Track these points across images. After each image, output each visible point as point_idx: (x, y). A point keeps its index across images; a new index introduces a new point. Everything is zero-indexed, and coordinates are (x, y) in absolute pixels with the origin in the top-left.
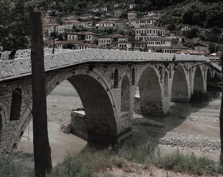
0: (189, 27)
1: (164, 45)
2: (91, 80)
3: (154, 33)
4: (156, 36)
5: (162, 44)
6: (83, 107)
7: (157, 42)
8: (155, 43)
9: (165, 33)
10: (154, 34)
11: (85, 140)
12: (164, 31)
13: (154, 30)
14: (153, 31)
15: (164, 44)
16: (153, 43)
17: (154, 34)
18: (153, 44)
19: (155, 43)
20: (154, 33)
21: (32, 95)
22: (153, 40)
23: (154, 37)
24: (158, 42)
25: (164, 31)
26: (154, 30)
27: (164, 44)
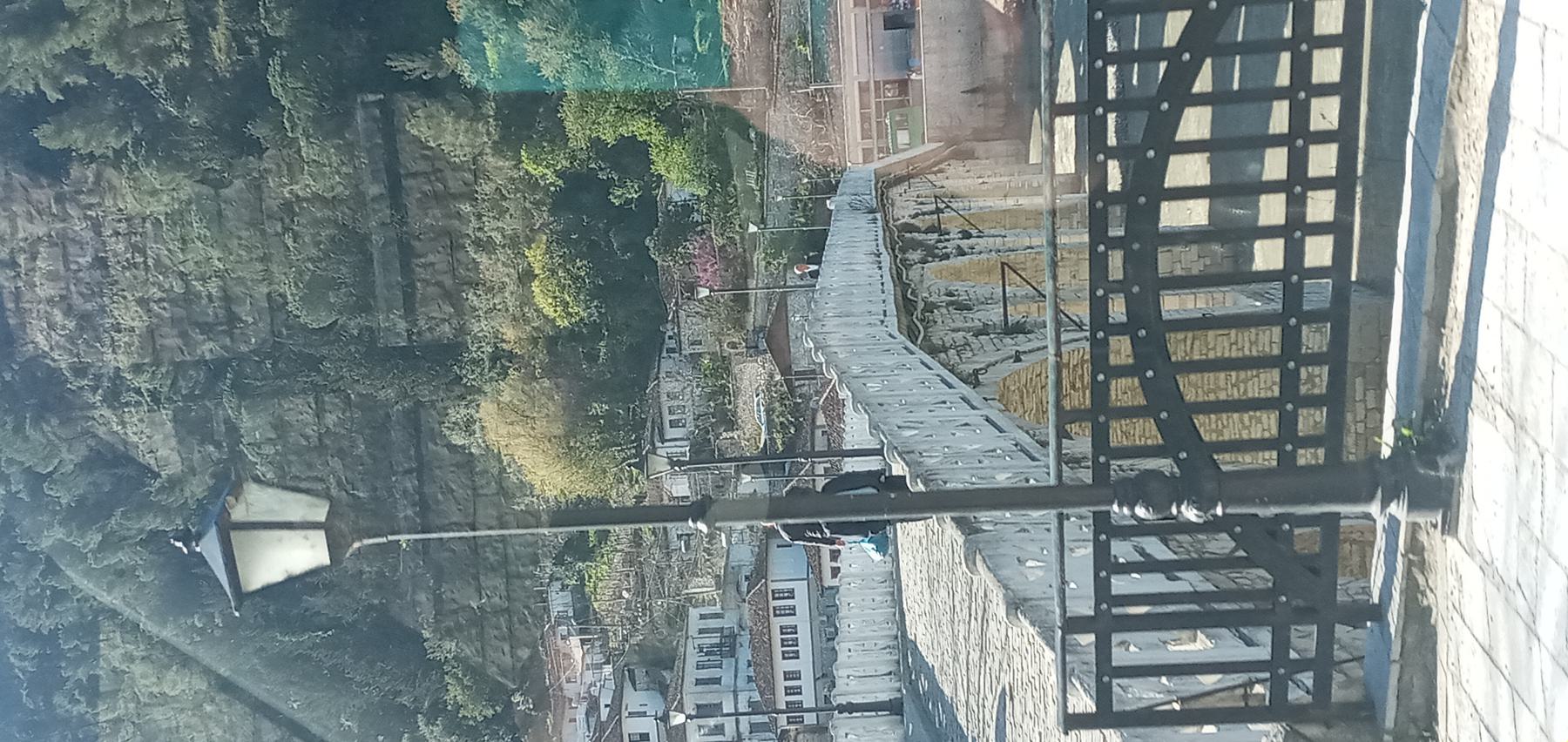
0: (663, 441)
1: (801, 588)
2: (1019, 378)
3: (717, 681)
4: (742, 665)
5: (792, 611)
6: (1142, 401)
7: (778, 650)
8: (791, 665)
9: (717, 609)
10: (727, 679)
11: (1166, 16)
12: (703, 617)
13: (699, 682)
14: (700, 688)
15: (791, 594)
16: (788, 676)
17: (727, 679)
18: (795, 675)
19: (791, 665)
20: (717, 681)
21: (1212, 416)
22: (768, 687)
23: (750, 679)
24: (777, 637)
25: (703, 617)
26: (699, 682)
27: (791, 594)
